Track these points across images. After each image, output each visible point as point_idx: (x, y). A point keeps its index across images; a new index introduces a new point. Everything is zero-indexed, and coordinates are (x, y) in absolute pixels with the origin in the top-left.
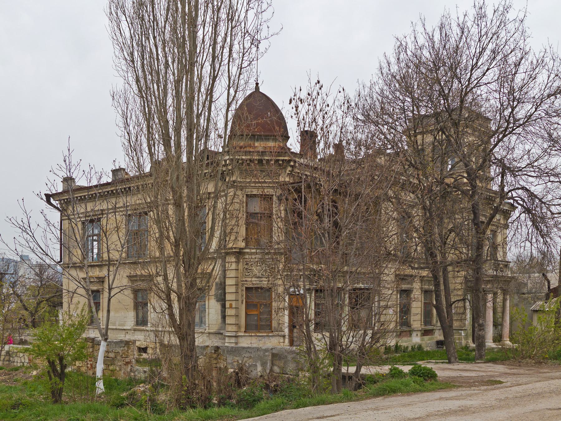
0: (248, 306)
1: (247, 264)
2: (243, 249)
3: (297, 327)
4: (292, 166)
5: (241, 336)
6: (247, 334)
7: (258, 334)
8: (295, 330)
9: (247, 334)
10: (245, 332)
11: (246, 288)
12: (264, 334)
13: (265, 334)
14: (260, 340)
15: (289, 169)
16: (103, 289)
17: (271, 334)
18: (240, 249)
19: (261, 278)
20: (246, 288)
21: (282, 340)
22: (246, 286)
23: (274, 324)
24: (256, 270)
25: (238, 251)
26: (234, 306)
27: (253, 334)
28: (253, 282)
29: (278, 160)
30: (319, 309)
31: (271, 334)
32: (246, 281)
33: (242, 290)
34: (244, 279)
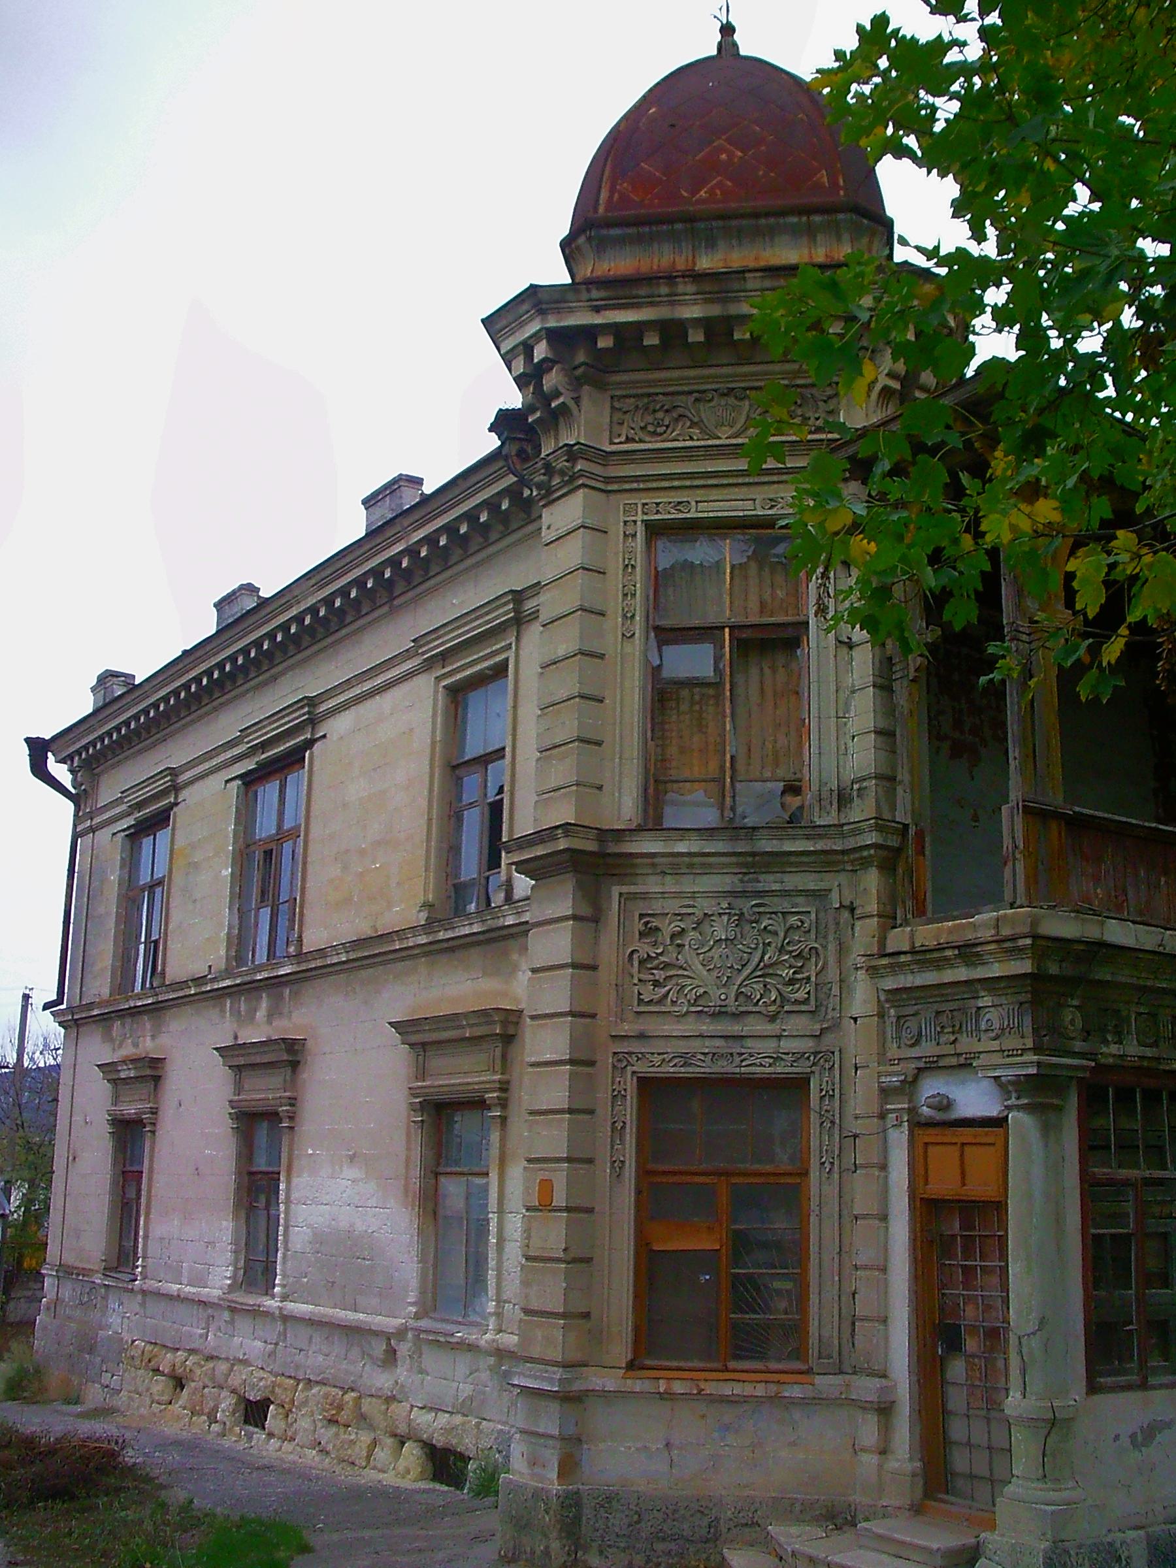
0: (656, 1196)
1: (649, 932)
2: (619, 835)
3: (971, 1344)
5: (604, 1394)
6: (638, 1386)
7: (710, 1388)
8: (957, 1369)
9: (638, 1386)
10: (631, 1366)
11: (644, 1083)
12: (748, 1389)
13: (760, 1390)
14: (726, 1428)
16: (504, 1087)
17: (795, 1392)
18: (603, 835)
19: (738, 1016)
20: (644, 1083)
21: (868, 1430)
22: (642, 1068)
23: (822, 1322)
24: (702, 971)
25: (591, 846)
26: (560, 1199)
27: (678, 1387)
28: (680, 1041)
30: (1118, 1218)
31: (795, 1392)
32: (642, 1036)
33: (617, 1097)
34: (626, 1028)
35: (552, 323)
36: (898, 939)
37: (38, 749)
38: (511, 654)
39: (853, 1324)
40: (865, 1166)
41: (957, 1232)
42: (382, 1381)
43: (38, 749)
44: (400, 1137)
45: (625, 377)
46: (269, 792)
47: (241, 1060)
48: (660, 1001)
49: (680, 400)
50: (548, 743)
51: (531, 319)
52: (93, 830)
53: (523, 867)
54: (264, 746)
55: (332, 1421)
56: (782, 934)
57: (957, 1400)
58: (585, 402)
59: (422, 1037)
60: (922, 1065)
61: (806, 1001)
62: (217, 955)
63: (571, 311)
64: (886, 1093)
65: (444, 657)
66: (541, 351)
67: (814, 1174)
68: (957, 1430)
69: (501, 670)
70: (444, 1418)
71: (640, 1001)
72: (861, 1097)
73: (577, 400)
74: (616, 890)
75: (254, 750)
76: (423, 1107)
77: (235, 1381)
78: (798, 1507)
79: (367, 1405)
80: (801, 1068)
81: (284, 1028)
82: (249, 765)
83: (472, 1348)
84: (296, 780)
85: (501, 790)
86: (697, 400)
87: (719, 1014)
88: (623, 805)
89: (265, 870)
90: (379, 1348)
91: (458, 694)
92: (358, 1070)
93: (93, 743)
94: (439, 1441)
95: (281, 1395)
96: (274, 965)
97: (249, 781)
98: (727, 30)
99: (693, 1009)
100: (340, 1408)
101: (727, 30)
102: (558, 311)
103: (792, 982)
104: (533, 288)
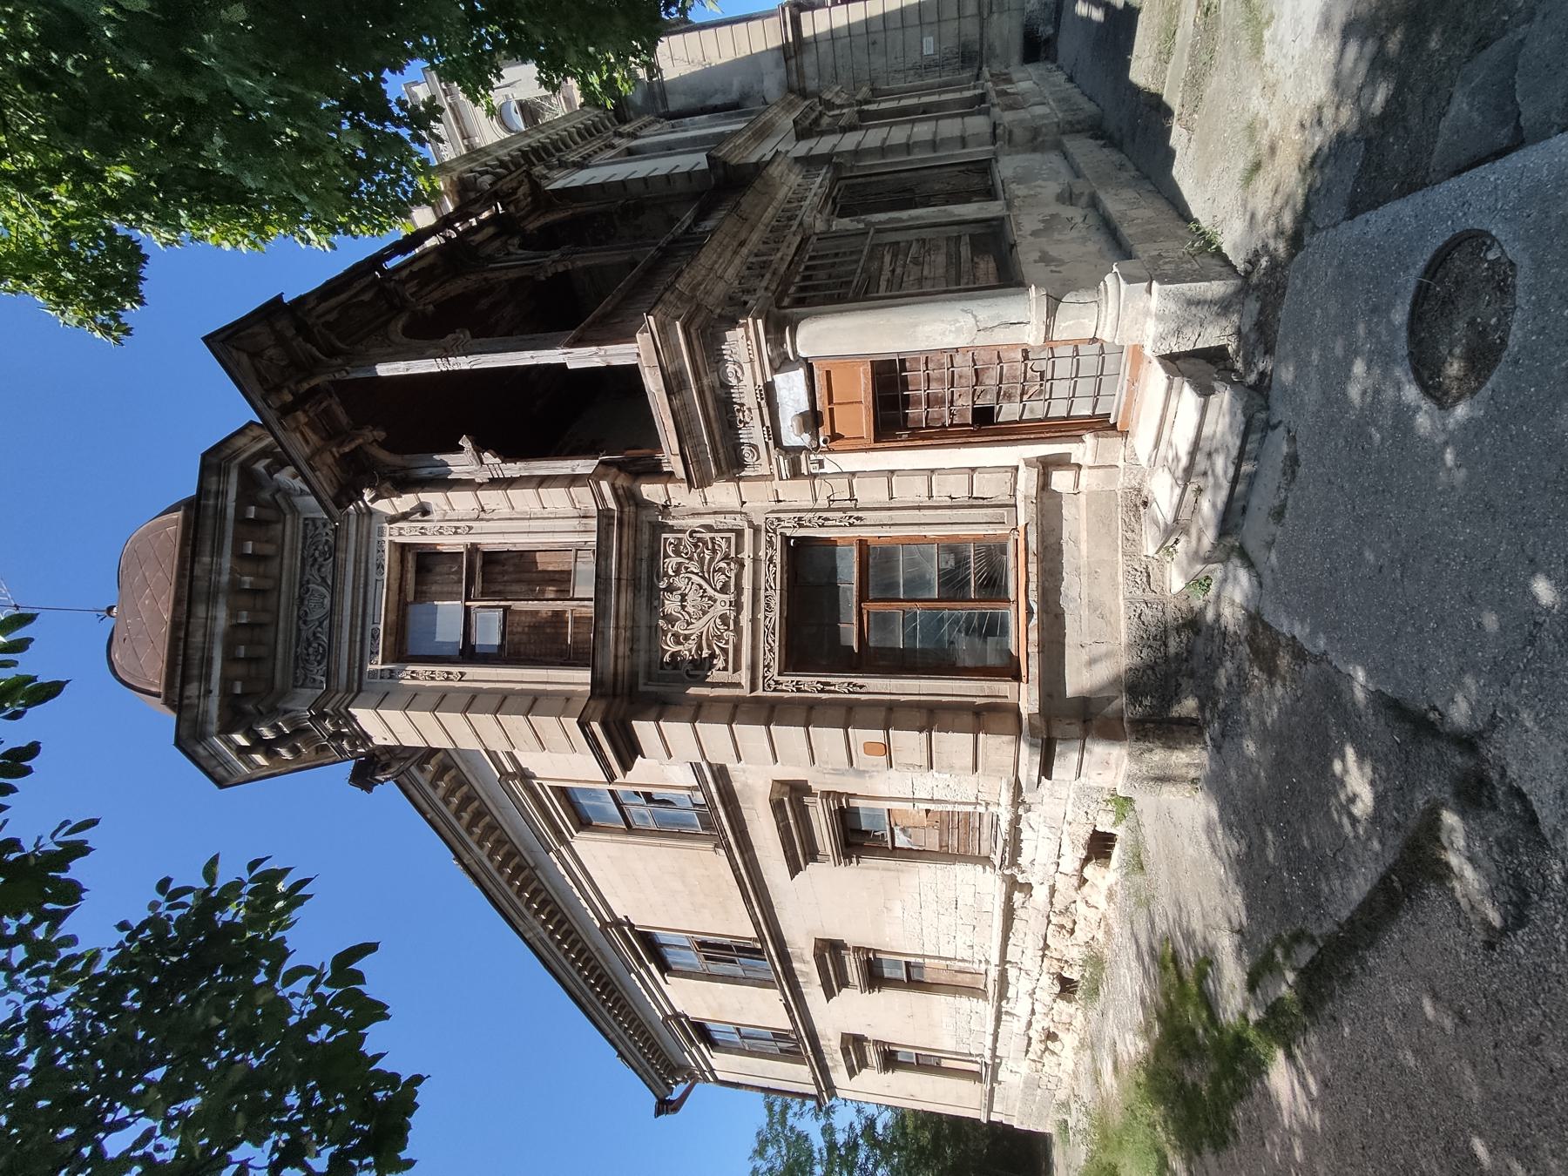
4: (271, 470)
15: (285, 477)
21: (1061, 480)
29: (241, 519)
35: (214, 727)
36: (674, 464)
37: (665, 1106)
38: (545, 784)
39: (985, 329)
40: (852, 494)
41: (894, 405)
42: (1040, 893)
43: (665, 1106)
44: (875, 875)
45: (278, 676)
46: (672, 957)
47: (833, 983)
48: (725, 651)
49: (304, 634)
50: (534, 742)
51: (212, 746)
52: (712, 1070)
53: (626, 767)
54: (639, 958)
55: (1072, 932)
56: (680, 560)
57: (1036, 410)
58: (289, 706)
59: (800, 853)
60: (771, 443)
61: (728, 539)
62: (774, 996)
63: (206, 712)
64: (796, 473)
65: (558, 833)
66: (241, 740)
67: (864, 533)
68: (1059, 410)
69: (563, 793)
70: (1066, 849)
71: (725, 669)
72: (797, 494)
73: (286, 712)
74: (642, 688)
75: (642, 964)
76: (848, 857)
77: (1048, 1000)
78: (1129, 535)
79: (1058, 906)
80: (778, 542)
81: (809, 955)
82: (653, 967)
83: (1016, 820)
84: (663, 937)
85: (636, 793)
86: (305, 622)
87: (737, 605)
88: (579, 679)
89: (720, 956)
90: (1018, 897)
91: (584, 823)
92: (824, 901)
93: (656, 1071)
94: (1083, 853)
95: (1055, 968)
96: (757, 954)
97: (665, 968)
99: (303, 198)
100: (1062, 927)
102: (205, 722)
103: (714, 551)
104: (179, 743)
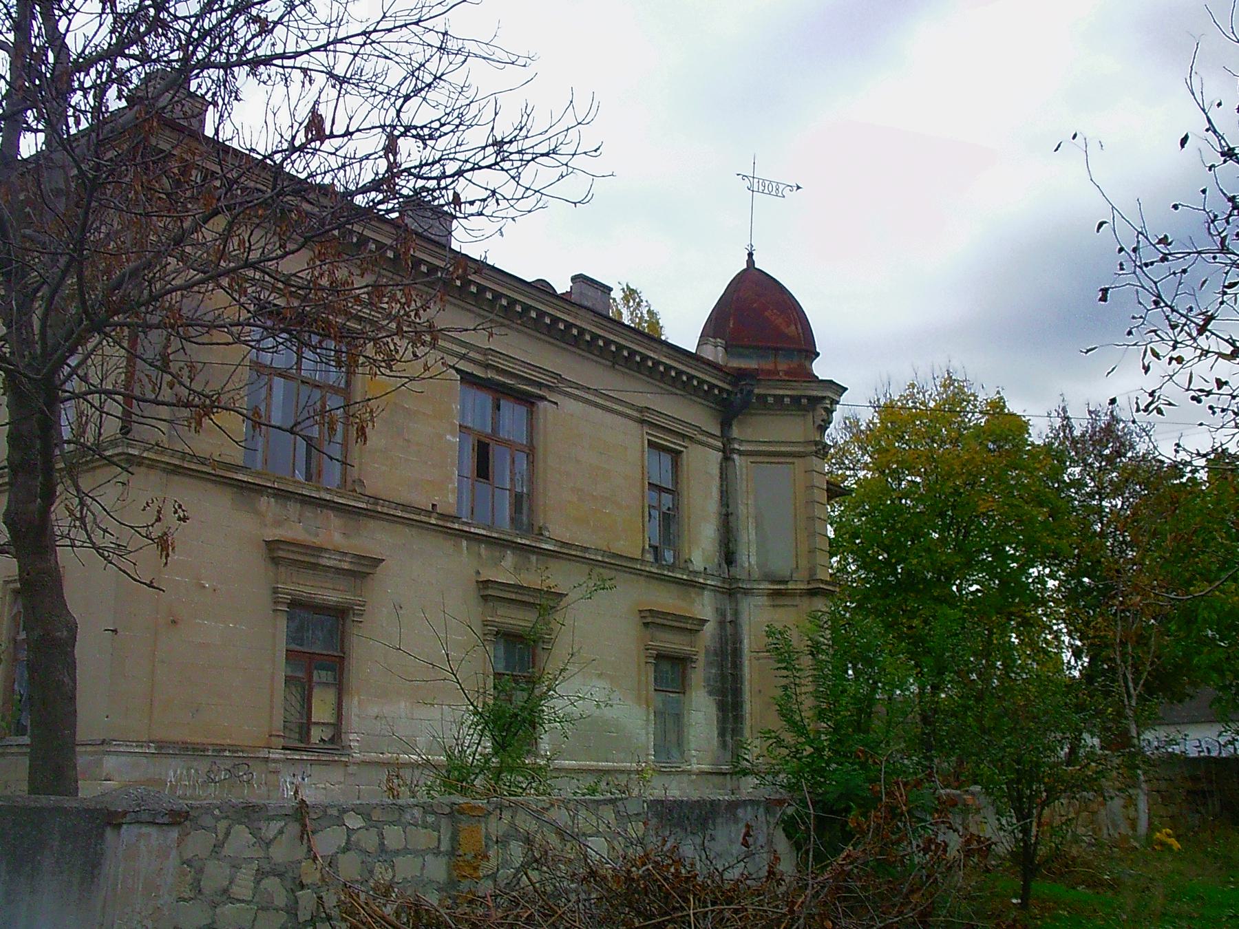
98: (750, 255)
101: (750, 255)
